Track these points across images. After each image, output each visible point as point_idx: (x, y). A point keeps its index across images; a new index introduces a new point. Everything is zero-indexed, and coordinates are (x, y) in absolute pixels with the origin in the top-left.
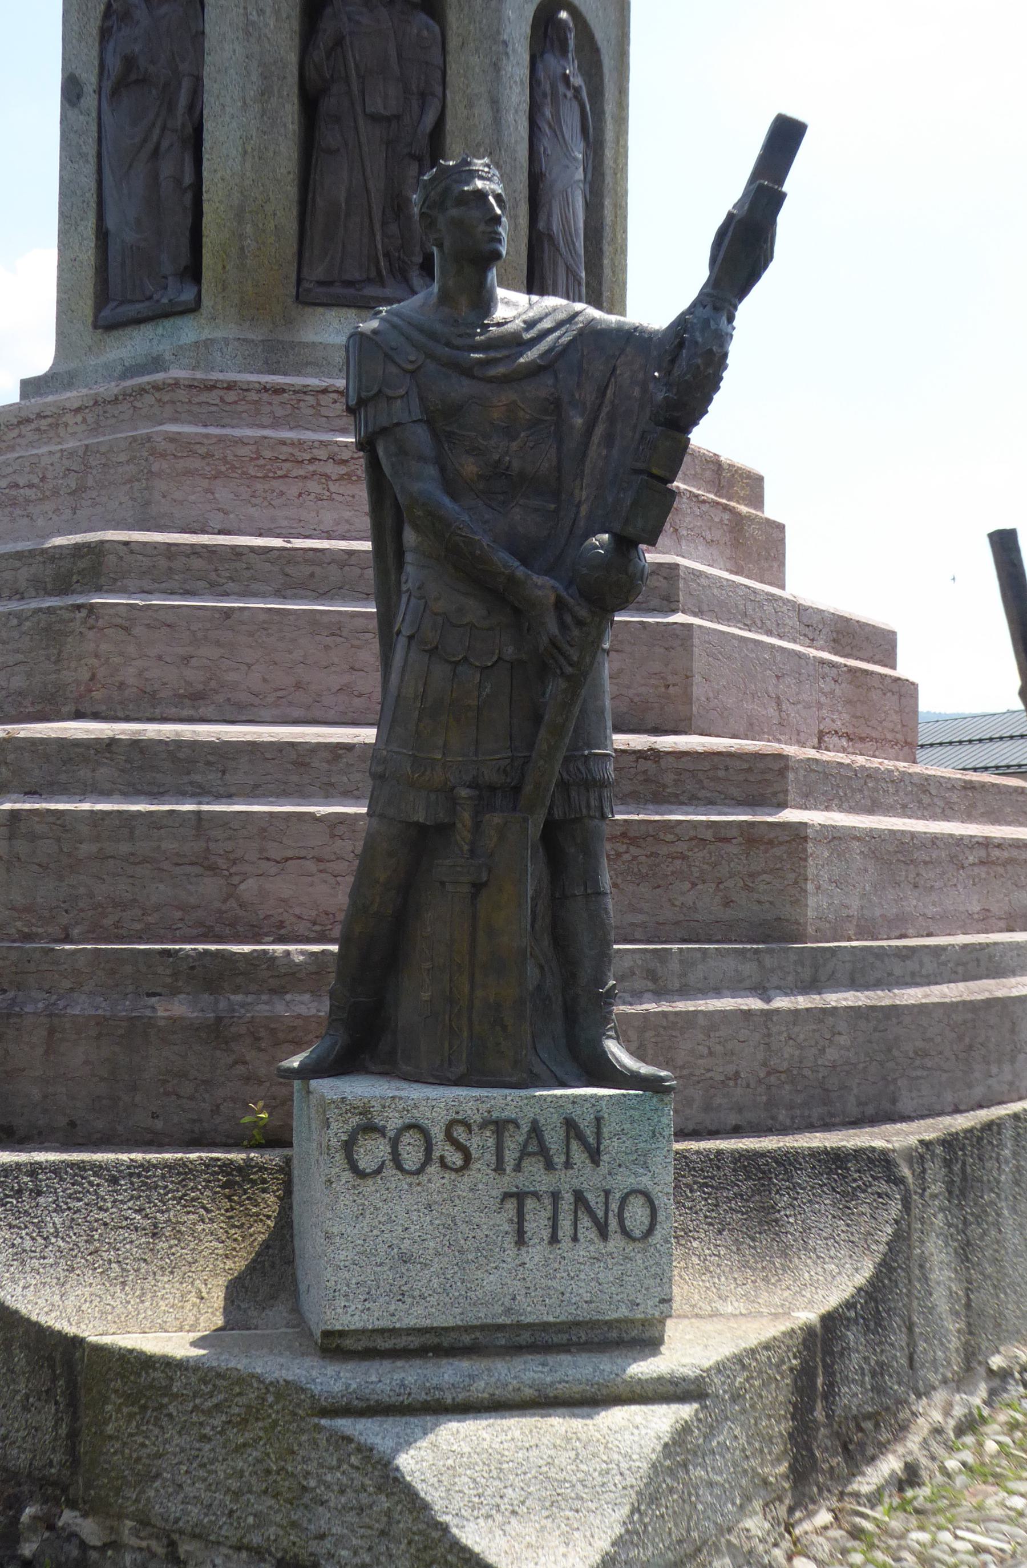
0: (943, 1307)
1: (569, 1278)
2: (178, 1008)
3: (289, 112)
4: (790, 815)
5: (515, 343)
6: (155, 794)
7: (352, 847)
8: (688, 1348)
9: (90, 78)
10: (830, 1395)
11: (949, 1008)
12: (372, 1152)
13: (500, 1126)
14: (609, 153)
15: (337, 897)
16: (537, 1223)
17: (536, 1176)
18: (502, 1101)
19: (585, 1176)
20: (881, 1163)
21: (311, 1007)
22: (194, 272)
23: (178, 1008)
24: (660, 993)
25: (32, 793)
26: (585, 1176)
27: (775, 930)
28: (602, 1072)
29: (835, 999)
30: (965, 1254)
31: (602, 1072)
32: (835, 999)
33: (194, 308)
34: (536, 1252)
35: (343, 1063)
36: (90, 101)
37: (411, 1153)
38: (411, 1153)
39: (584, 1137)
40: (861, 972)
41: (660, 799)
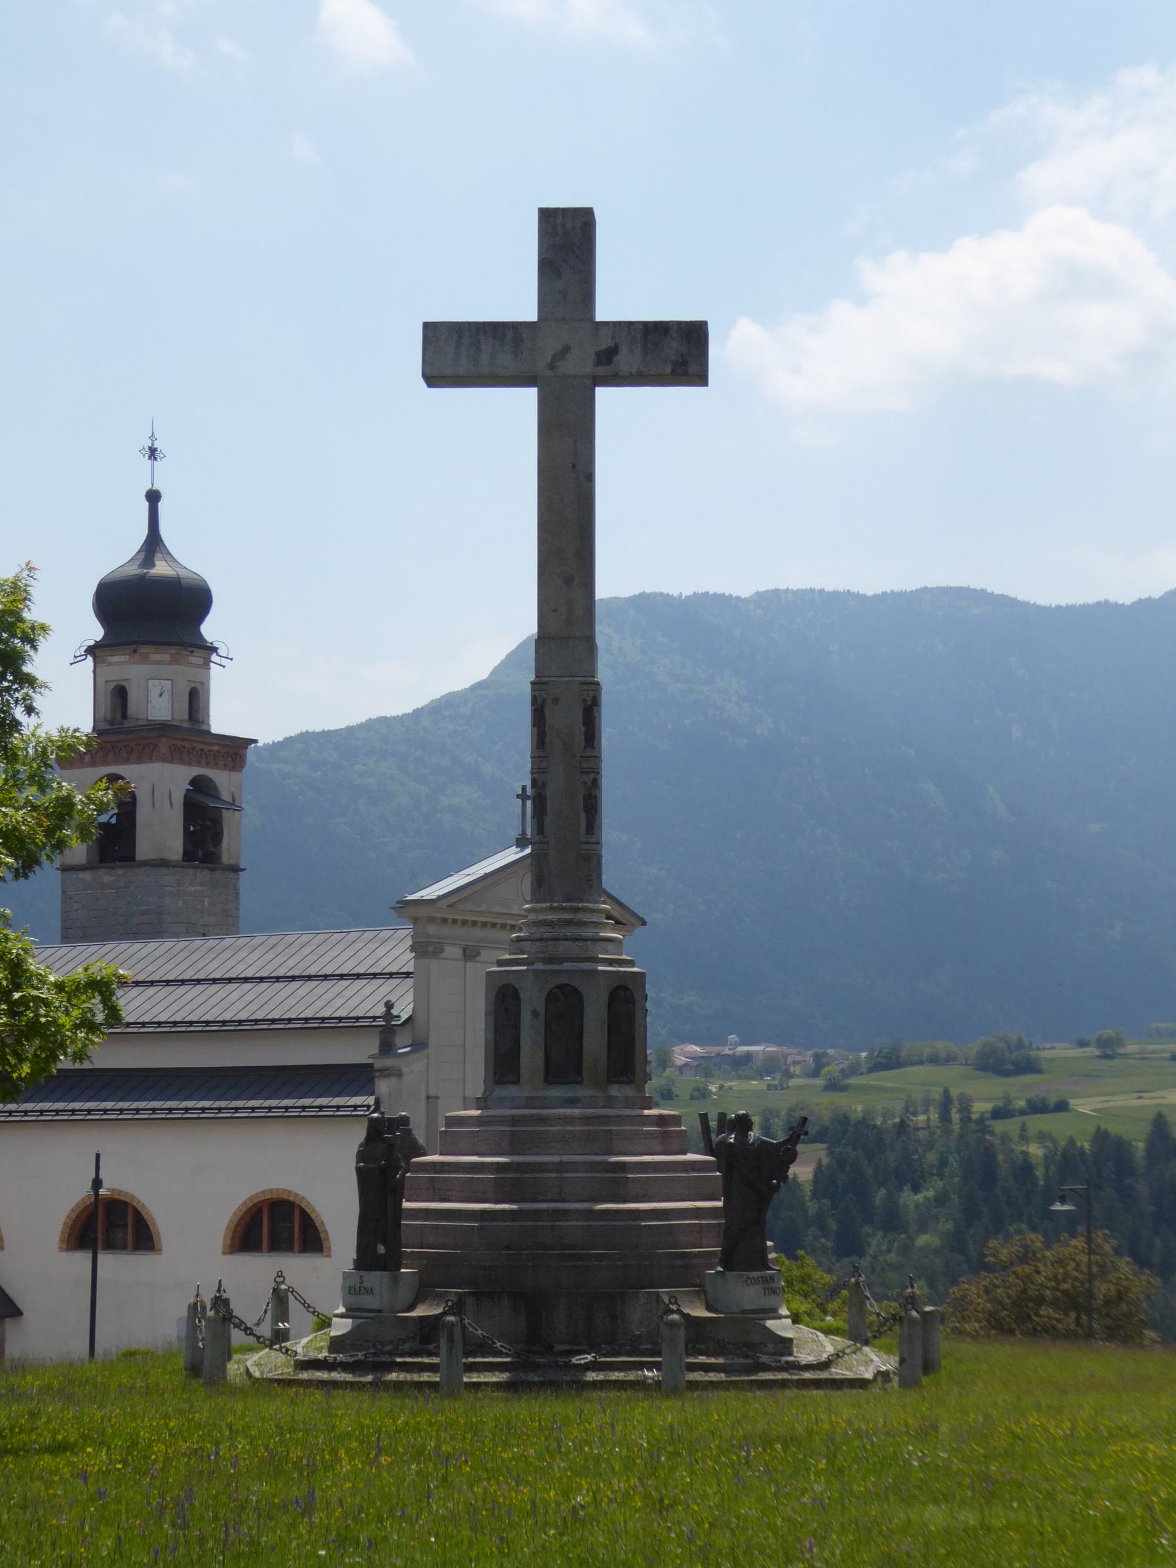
2: (679, 1262)
5: (753, 1144)
23: (679, 1262)
26: (772, 1285)
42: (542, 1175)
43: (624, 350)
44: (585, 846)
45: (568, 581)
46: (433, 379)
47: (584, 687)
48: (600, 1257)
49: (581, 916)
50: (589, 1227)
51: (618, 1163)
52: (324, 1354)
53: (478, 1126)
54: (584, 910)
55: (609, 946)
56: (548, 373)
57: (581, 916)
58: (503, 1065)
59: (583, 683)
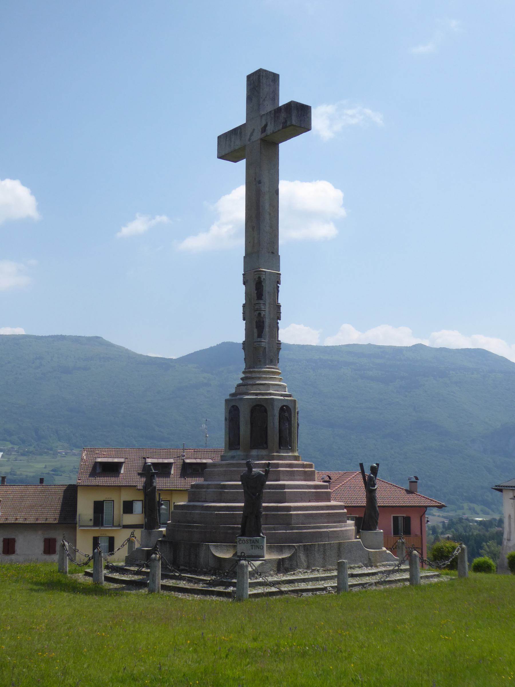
0: (303, 561)
1: (256, 552)
2: (230, 531)
3: (249, 426)
4: (291, 513)
5: (254, 476)
6: (229, 511)
7: (242, 516)
8: (267, 557)
9: (228, 418)
10: (283, 565)
11: (310, 532)
12: (241, 542)
13: (250, 540)
14: (293, 422)
15: (241, 520)
16: (254, 547)
17: (253, 544)
18: (251, 538)
19: (258, 544)
20: (294, 546)
21: (239, 531)
22: (239, 444)
23: (230, 531)
24: (275, 530)
25: (218, 511)
26: (258, 544)
27: (289, 524)
28: (260, 536)
29: (294, 531)
30: (307, 556)
31: (260, 536)
32: (294, 531)
33: (239, 449)
34: (253, 550)
35: (241, 536)
36: (228, 421)
37: (244, 542)
38: (244, 542)
39: (257, 541)
40: (298, 528)
41: (278, 511)
42: (201, 490)
43: (269, 124)
44: (255, 344)
45: (253, 228)
46: (220, 157)
47: (255, 273)
48: (197, 527)
49: (254, 375)
50: (200, 513)
51: (224, 485)
52: (122, 564)
53: (280, 470)
54: (255, 372)
55: (261, 387)
56: (249, 143)
57: (254, 375)
58: (233, 441)
59: (255, 272)
